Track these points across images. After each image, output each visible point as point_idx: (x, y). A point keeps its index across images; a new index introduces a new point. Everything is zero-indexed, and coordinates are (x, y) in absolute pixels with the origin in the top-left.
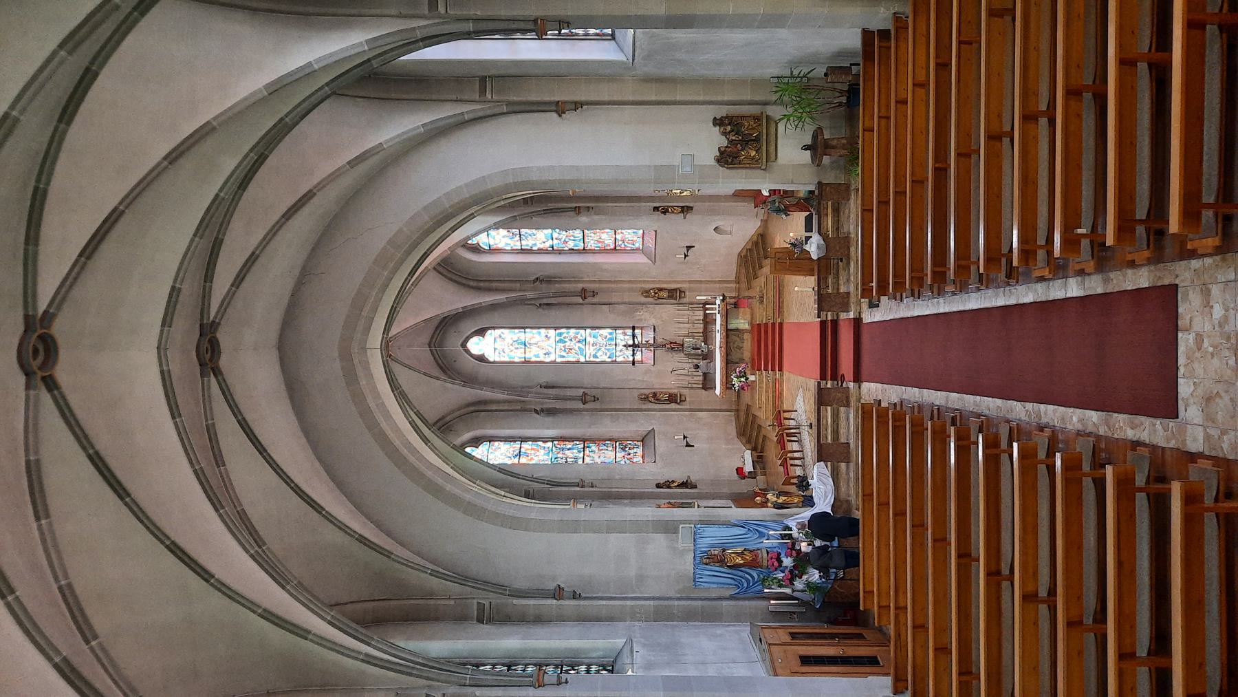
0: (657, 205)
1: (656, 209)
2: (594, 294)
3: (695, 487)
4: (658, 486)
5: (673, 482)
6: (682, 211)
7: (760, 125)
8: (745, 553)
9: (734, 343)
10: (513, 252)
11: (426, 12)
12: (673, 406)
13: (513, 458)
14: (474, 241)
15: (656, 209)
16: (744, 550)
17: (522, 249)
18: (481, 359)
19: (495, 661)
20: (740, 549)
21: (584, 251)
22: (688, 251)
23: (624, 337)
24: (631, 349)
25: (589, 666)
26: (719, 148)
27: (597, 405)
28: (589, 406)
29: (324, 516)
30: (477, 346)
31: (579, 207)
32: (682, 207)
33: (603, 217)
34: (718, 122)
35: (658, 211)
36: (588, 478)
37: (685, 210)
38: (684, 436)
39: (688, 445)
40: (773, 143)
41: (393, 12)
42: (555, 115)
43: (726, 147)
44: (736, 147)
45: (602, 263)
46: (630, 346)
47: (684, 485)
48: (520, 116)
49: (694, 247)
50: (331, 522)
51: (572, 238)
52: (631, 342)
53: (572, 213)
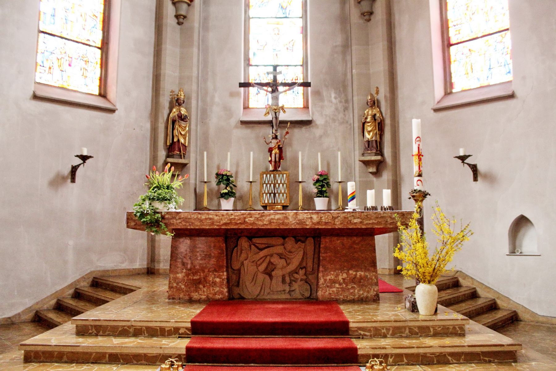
9: (281, 256)
39: (74, 170)
49: (475, 179)
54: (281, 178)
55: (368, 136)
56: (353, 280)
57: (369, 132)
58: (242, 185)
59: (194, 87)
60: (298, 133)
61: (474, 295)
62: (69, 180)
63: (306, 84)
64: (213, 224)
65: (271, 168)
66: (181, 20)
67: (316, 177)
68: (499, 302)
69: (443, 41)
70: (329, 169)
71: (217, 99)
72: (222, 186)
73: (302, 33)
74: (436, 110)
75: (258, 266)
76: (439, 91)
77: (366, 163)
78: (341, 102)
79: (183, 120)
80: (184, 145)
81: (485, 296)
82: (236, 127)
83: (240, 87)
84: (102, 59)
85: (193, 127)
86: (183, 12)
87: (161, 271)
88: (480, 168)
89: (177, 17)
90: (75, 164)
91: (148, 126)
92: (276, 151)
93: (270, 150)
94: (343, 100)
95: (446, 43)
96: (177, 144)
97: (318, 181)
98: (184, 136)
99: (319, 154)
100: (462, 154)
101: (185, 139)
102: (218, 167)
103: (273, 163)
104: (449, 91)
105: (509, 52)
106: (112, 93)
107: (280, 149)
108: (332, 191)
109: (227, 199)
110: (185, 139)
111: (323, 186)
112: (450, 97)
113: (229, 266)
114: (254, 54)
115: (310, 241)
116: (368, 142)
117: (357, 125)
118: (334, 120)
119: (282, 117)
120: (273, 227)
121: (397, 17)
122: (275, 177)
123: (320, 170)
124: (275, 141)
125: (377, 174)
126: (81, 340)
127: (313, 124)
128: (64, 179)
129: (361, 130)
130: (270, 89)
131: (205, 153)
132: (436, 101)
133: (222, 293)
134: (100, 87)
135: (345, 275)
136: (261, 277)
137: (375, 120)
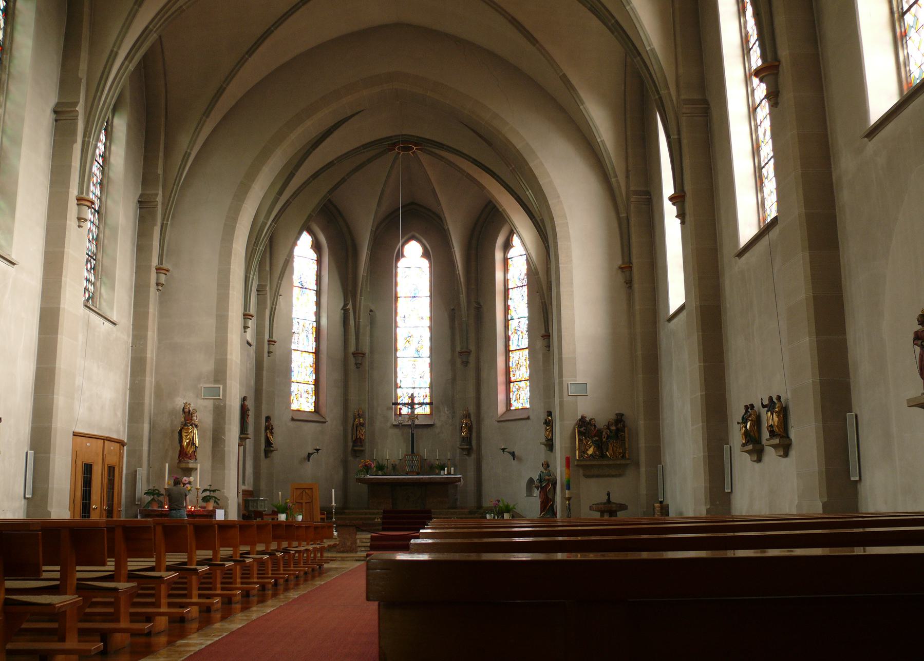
2: (466, 363)
3: (266, 456)
4: (268, 419)
5: (272, 433)
6: (548, 440)
10: (506, 282)
11: (683, 97)
12: (350, 444)
13: (300, 281)
14: (516, 240)
18: (400, 255)
19: (104, 199)
21: (507, 351)
22: (509, 452)
23: (423, 394)
24: (410, 402)
25: (94, 284)
27: (352, 367)
28: (352, 360)
29: (244, 56)
30: (413, 251)
33: (541, 364)
34: (619, 419)
35: (548, 416)
38: (319, 450)
39: (309, 455)
41: (681, 71)
42: (620, 262)
43: (595, 426)
46: (413, 400)
47: (268, 443)
49: (514, 459)
50: (237, 64)
51: (520, 337)
52: (416, 401)
53: (543, 332)
62: (307, 460)
66: (359, 366)
74: (499, 422)
76: (501, 408)
77: (463, 449)
79: (362, 426)
80: (363, 440)
82: (390, 428)
83: (393, 405)
85: (367, 428)
89: (356, 364)
105: (528, 398)
106: (323, 410)
116: (463, 437)
119: (417, 422)
122: (412, 458)
125: (469, 454)
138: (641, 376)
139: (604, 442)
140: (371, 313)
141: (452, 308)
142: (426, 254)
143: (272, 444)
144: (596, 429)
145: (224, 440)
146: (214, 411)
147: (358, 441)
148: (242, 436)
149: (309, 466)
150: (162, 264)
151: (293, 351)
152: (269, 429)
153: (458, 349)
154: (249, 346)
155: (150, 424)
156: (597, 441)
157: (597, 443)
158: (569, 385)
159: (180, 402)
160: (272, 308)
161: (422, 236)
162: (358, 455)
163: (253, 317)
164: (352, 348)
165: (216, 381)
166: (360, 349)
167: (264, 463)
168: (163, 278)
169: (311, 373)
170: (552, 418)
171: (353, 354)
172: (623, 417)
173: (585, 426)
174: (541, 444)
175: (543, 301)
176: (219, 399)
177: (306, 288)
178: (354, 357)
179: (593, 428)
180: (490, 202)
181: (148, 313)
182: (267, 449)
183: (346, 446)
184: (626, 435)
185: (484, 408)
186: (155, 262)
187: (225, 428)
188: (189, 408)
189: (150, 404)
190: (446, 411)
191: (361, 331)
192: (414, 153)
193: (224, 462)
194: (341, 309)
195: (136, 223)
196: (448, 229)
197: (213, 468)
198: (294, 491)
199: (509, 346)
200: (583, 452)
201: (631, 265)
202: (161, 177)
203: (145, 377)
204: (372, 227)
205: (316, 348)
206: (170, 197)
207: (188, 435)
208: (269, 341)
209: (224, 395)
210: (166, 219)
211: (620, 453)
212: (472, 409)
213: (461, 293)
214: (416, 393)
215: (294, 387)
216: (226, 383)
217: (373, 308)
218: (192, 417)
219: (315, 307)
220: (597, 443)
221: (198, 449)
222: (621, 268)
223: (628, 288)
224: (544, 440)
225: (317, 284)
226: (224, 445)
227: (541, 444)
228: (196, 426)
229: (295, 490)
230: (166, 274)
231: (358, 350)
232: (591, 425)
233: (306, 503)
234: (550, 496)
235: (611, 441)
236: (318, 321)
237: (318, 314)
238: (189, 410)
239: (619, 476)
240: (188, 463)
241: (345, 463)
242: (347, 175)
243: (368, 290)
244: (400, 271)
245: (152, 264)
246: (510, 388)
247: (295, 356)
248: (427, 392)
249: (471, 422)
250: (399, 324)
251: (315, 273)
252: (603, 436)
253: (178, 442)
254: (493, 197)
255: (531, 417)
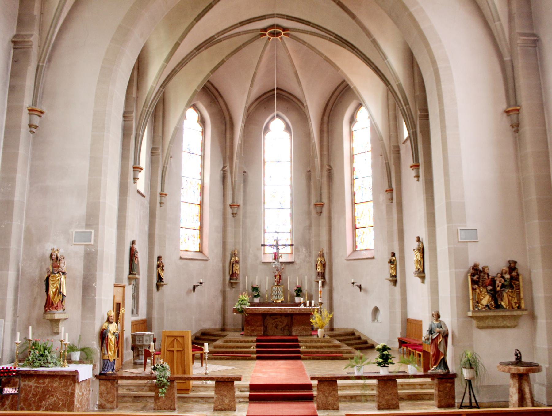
0: (397, 255)
1: (393, 255)
4: (159, 258)
5: (163, 270)
7: (513, 308)
8: (61, 296)
9: (280, 322)
10: (351, 149)
12: (228, 278)
15: (393, 255)
16: (63, 295)
17: (354, 155)
20: (64, 291)
22: (357, 285)
23: (286, 238)
24: (275, 243)
26: (487, 267)
27: (229, 216)
28: (229, 211)
31: (392, 190)
32: (395, 276)
34: (512, 267)
36: (168, 200)
37: (394, 280)
39: (194, 287)
40: (494, 323)
42: (504, 106)
44: (489, 285)
45: (345, 218)
46: (277, 243)
47: (160, 279)
48: (500, 75)
49: (361, 291)
52: (280, 243)
53: (386, 187)
54: (281, 289)
55: (318, 270)
56: (303, 329)
57: (319, 269)
58: (263, 290)
59: (241, 247)
60: (288, 267)
61: (359, 338)
62: (193, 291)
63: (292, 245)
64: (259, 311)
65: (276, 284)
67: (296, 288)
68: (368, 341)
69: (353, 226)
70: (302, 284)
71: (251, 251)
72: (255, 292)
73: (290, 216)
75: (273, 325)
76: (349, 249)
78: (307, 253)
79: (237, 263)
80: (238, 274)
81: (363, 338)
84: (200, 235)
85: (241, 265)
86: (235, 212)
87: (228, 329)
88: (362, 286)
89: (233, 214)
90: (195, 285)
91: (221, 265)
92: (278, 277)
93: (276, 276)
94: (309, 252)
95: (354, 227)
96: (234, 274)
97: (296, 290)
98: (238, 270)
99: (297, 277)
100: (352, 282)
101: (238, 271)
102: (252, 283)
103: (277, 282)
104: (354, 250)
106: (206, 251)
107: (280, 276)
108: (303, 294)
109: (257, 298)
110: (238, 271)
111: (298, 292)
112: (356, 253)
113: (264, 325)
114: (268, 227)
115: (289, 317)
116: (319, 273)
117: (314, 265)
118: (304, 261)
120: (278, 312)
121: (333, 214)
123: (298, 284)
124: (277, 272)
126: (215, 349)
127: (295, 263)
128: (191, 291)
129: (316, 267)
130: (275, 248)
131: (247, 277)
132: (347, 256)
133: (261, 333)
134: (200, 248)
135: (301, 328)
136: (274, 328)
137: (321, 263)
138: (536, 221)
139: (499, 291)
140: (244, 174)
141: (308, 170)
142: (288, 128)
143: (163, 279)
144: (490, 277)
145: (95, 289)
146: (85, 257)
147: (233, 276)
148: (131, 276)
149: (194, 295)
150: (36, 106)
151: (182, 203)
152: (160, 266)
153: (313, 202)
154: (143, 198)
155: (18, 271)
156: (490, 290)
157: (492, 292)
158: (459, 231)
159: (48, 248)
160: (164, 167)
161: (285, 114)
162: (233, 286)
163: (142, 169)
164: (229, 201)
165: (88, 226)
166: (235, 202)
167: (156, 295)
168: (36, 120)
169: (197, 220)
170: (395, 258)
171: (231, 206)
172: (516, 264)
173: (477, 274)
174: (386, 279)
175: (387, 162)
176: (91, 245)
177: (193, 153)
178: (231, 208)
179: (486, 277)
180: (344, 81)
181: (17, 154)
182: (158, 283)
183: (224, 280)
184: (521, 284)
185: (335, 249)
186: (27, 102)
187: (96, 275)
188: (57, 254)
189: (18, 251)
190: (303, 250)
191: (237, 187)
192: (281, 38)
193: (95, 312)
194: (221, 171)
195: (8, 64)
196: (307, 106)
197: (83, 317)
198: (165, 339)
199: (354, 199)
200: (477, 302)
201: (518, 108)
202: (37, 18)
203: (12, 221)
204: (246, 103)
205: (200, 201)
206: (47, 38)
207: (54, 284)
208: (161, 194)
209: (96, 240)
210: (41, 61)
211: (516, 303)
212: (325, 251)
213: (316, 157)
214: (280, 236)
215: (182, 232)
216: (98, 227)
217: (246, 170)
218: (59, 264)
219: (201, 168)
220: (492, 292)
221: (66, 299)
222: (507, 112)
223: (514, 131)
224: (388, 277)
225: (202, 151)
226: (95, 294)
227: (386, 279)
228: (64, 273)
229: (166, 338)
230: (40, 116)
231: (234, 203)
232: (485, 273)
233: (177, 351)
234: (442, 350)
235: (507, 290)
236: (202, 180)
237: (202, 174)
238: (57, 257)
239: (514, 327)
240: (54, 314)
241: (224, 293)
242: (226, 57)
243: (243, 155)
244: (267, 142)
245: (24, 104)
246: (355, 233)
247: (183, 206)
248: (288, 236)
249: (325, 261)
250: (266, 183)
251: (201, 142)
252: (497, 285)
253: (45, 291)
254: (346, 76)
255: (375, 257)
